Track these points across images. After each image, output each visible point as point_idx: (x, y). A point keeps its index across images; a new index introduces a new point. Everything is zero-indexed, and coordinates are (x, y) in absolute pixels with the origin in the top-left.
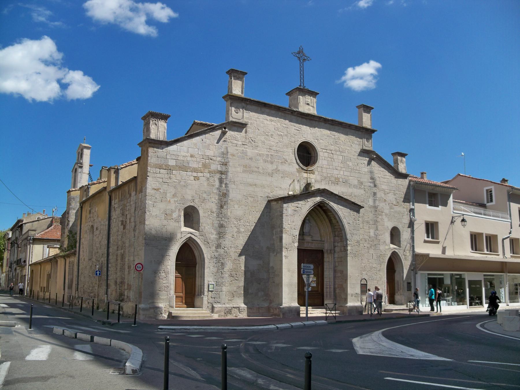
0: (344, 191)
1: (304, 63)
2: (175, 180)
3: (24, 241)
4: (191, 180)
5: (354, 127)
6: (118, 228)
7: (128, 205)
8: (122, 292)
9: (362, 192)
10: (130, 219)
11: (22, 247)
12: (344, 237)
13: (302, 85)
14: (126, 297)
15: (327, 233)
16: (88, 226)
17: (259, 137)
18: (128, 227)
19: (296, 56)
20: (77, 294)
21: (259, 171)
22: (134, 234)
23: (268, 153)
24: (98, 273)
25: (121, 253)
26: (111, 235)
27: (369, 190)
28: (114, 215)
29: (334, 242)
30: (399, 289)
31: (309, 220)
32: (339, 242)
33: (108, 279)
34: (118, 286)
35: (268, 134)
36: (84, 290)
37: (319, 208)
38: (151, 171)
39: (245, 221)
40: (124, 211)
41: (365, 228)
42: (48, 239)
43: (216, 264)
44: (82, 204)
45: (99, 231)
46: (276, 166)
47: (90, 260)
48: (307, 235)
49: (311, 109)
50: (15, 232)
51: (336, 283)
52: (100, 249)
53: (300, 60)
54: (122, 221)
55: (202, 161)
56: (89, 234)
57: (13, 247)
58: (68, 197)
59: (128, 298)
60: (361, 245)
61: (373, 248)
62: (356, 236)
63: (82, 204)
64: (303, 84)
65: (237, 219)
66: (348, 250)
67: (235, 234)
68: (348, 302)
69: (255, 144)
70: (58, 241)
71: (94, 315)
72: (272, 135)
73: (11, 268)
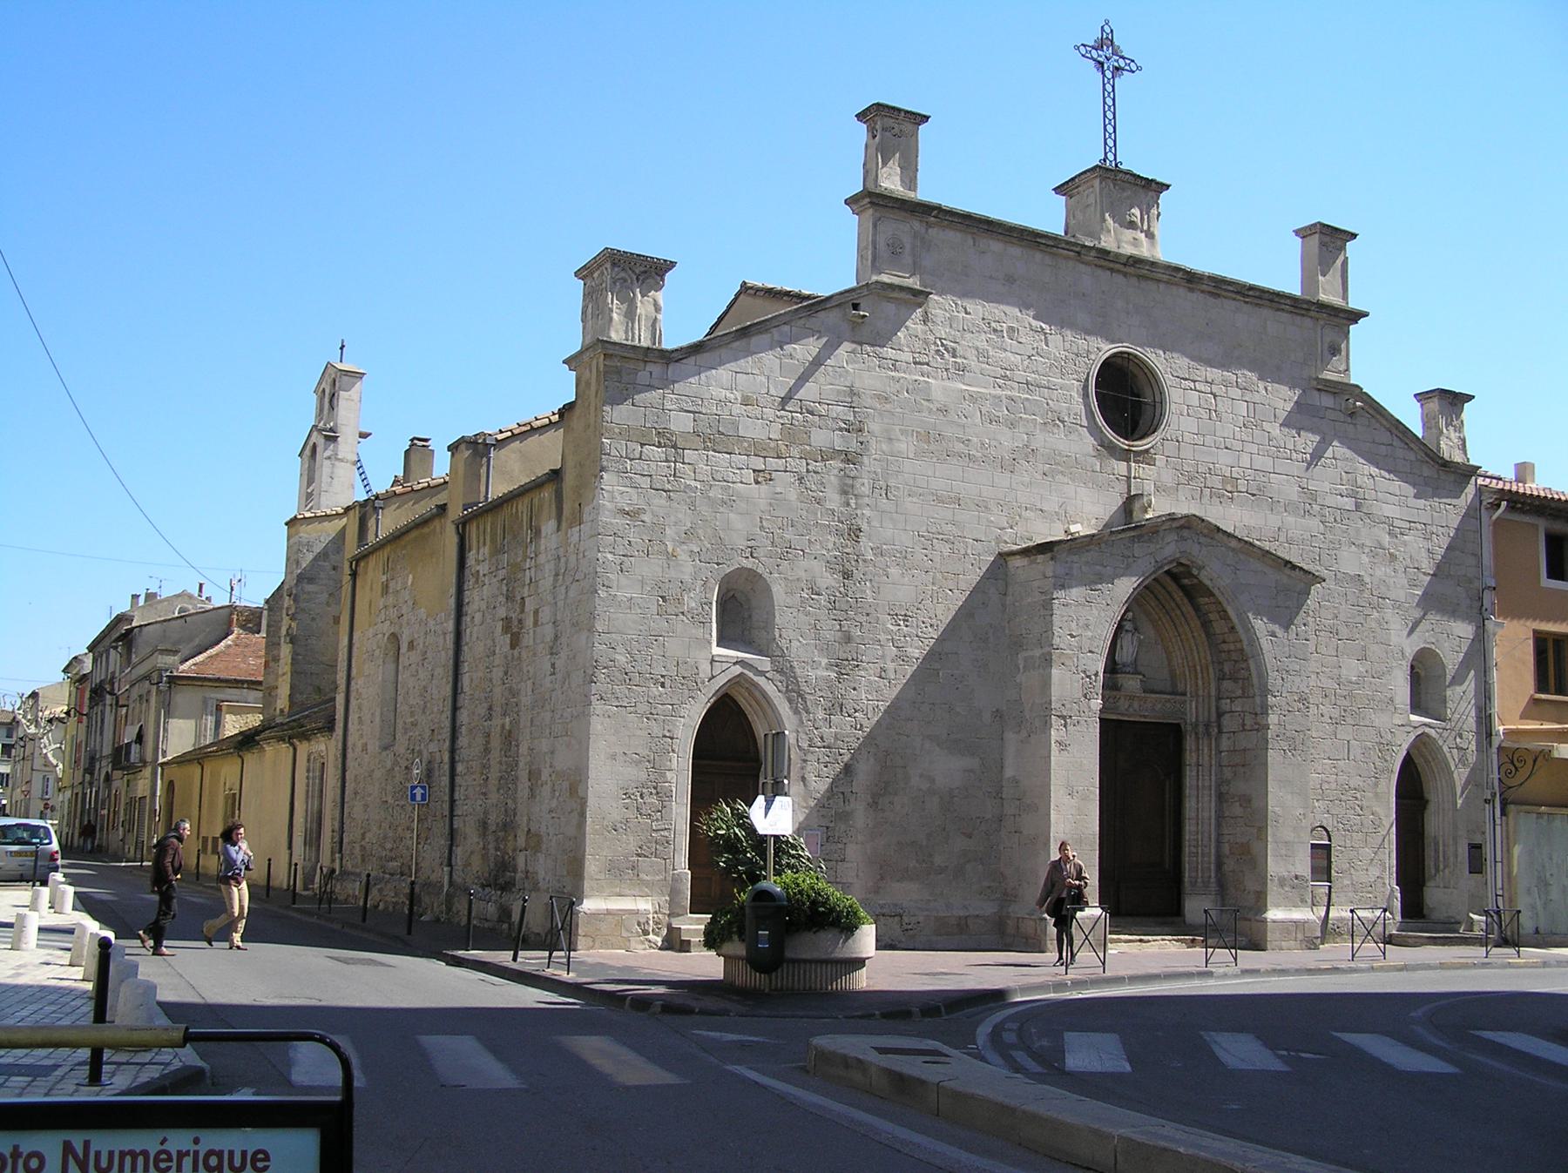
0: (1252, 523)
1: (1117, 80)
2: (693, 483)
3: (137, 685)
4: (746, 487)
5: (1288, 302)
6: (489, 642)
7: (528, 566)
8: (507, 857)
9: (1314, 524)
10: (536, 612)
11: (131, 707)
12: (1255, 681)
13: (1111, 157)
14: (519, 875)
15: (1195, 666)
16: (380, 636)
17: (968, 336)
18: (527, 640)
19: (1089, 55)
20: (338, 861)
21: (971, 453)
22: (553, 665)
23: (999, 392)
24: (419, 792)
25: (503, 726)
26: (465, 668)
27: (1338, 519)
28: (477, 598)
29: (1219, 699)
30: (1441, 867)
31: (1133, 620)
32: (1236, 698)
33: (455, 813)
34: (491, 838)
35: (999, 328)
36: (363, 848)
37: (1172, 586)
38: (614, 452)
39: (924, 623)
40: (514, 588)
41: (1322, 649)
42: (218, 680)
43: (826, 767)
44: (354, 563)
45: (418, 651)
46: (1026, 436)
47: (386, 748)
48: (1129, 673)
49: (1142, 242)
50: (104, 655)
51: (1226, 838)
52: (424, 712)
53: (1103, 73)
54: (507, 621)
55: (782, 417)
56: (381, 663)
57: (97, 704)
58: (288, 540)
59: (527, 877)
60: (1313, 709)
61: (1350, 720)
62: (1297, 680)
63: (354, 563)
64: (1115, 155)
65: (896, 615)
66: (1271, 727)
67: (891, 666)
68: (1268, 905)
69: (956, 362)
70: (253, 685)
71: (413, 933)
72: (1011, 329)
73: (92, 774)
